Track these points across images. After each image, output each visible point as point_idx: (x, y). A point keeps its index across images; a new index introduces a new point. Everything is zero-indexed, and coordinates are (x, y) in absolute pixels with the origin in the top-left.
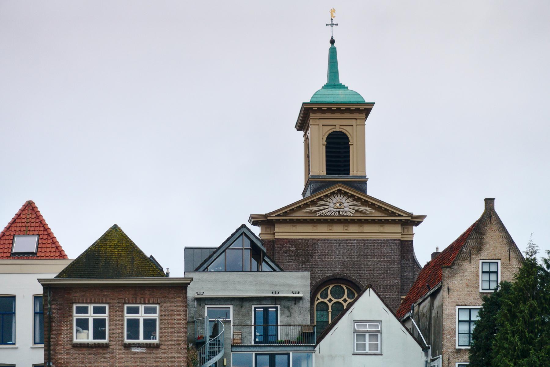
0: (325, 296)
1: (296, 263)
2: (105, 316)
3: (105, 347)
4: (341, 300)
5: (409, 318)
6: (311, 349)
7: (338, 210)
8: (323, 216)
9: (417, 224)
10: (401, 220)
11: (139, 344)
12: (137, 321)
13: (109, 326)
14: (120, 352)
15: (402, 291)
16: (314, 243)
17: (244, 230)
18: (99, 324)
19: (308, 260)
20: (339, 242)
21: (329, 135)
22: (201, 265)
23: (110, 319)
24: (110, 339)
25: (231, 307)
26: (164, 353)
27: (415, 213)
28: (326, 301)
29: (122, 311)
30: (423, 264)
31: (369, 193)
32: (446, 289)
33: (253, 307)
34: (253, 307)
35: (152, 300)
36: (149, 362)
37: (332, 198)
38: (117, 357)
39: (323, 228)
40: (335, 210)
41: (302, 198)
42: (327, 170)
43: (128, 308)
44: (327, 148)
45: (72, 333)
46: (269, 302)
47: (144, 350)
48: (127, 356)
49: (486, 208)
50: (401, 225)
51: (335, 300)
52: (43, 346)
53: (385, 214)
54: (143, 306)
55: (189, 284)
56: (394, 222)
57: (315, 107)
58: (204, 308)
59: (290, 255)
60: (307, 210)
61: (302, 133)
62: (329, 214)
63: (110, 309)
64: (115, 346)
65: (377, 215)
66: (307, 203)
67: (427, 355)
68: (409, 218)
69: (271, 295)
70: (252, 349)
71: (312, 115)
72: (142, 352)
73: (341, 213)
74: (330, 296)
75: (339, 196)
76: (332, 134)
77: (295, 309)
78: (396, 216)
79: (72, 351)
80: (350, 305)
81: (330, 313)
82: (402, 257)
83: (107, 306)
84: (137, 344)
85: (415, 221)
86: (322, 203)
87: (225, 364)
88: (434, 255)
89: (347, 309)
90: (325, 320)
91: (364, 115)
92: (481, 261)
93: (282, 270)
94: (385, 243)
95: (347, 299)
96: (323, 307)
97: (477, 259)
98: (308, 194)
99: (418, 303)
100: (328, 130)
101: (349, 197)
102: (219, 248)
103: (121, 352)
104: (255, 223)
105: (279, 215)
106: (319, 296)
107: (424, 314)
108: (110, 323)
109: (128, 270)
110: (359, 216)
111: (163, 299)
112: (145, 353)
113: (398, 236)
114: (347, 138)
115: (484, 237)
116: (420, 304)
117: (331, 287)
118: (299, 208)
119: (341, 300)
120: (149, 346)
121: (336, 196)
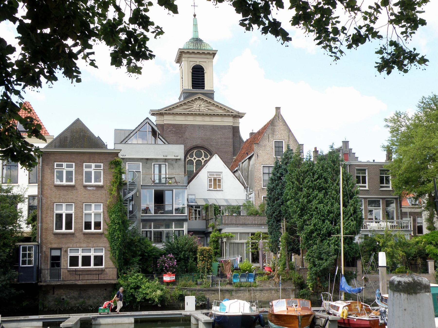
0: (192, 156)
3: (73, 187)
4: (200, 159)
5: (237, 170)
6: (185, 187)
7: (198, 108)
8: (190, 112)
9: (241, 117)
10: (233, 115)
13: (75, 175)
15: (234, 154)
16: (186, 126)
17: (147, 120)
18: (69, 174)
19: (182, 136)
20: (199, 126)
22: (124, 140)
23: (75, 171)
24: (75, 183)
25: (141, 163)
27: (240, 112)
28: (192, 159)
29: (83, 167)
30: (245, 140)
31: (215, 99)
32: (256, 156)
33: (153, 163)
34: (153, 163)
35: (99, 161)
36: (97, 195)
37: (195, 101)
38: (79, 192)
39: (190, 118)
40: (197, 108)
41: (178, 101)
43: (85, 165)
44: (192, 73)
45: (54, 178)
46: (162, 161)
47: (94, 188)
48: (85, 192)
49: (276, 112)
50: (233, 118)
51: (197, 159)
52: (37, 184)
53: (224, 111)
55: (119, 152)
57: (186, 51)
58: (126, 164)
60: (182, 108)
61: (178, 64)
63: (75, 165)
64: (79, 187)
65: (220, 112)
66: (181, 104)
67: (247, 191)
68: (237, 114)
69: (163, 157)
70: (152, 187)
71: (184, 55)
72: (93, 190)
73: (200, 110)
74: (194, 157)
75: (199, 100)
76: (185, 153)
77: (176, 165)
78: (230, 113)
79: (54, 189)
80: (206, 162)
81: (195, 166)
82: (234, 135)
83: (74, 164)
86: (190, 104)
87: (138, 196)
88: (251, 134)
89: (204, 165)
90: (192, 170)
91: (212, 56)
93: (169, 144)
94: (224, 127)
95: (204, 158)
96: (191, 162)
97: (272, 139)
98: (182, 99)
99: (242, 162)
100: (193, 64)
101: (204, 101)
102: (134, 130)
103: (81, 190)
104: (153, 114)
105: (166, 110)
106: (188, 156)
107: (245, 169)
108: (75, 173)
110: (210, 112)
111: (105, 160)
112: (95, 190)
113: (231, 124)
114: (203, 69)
115: (276, 128)
116: (243, 163)
117: (195, 151)
119: (200, 159)
121: (197, 101)
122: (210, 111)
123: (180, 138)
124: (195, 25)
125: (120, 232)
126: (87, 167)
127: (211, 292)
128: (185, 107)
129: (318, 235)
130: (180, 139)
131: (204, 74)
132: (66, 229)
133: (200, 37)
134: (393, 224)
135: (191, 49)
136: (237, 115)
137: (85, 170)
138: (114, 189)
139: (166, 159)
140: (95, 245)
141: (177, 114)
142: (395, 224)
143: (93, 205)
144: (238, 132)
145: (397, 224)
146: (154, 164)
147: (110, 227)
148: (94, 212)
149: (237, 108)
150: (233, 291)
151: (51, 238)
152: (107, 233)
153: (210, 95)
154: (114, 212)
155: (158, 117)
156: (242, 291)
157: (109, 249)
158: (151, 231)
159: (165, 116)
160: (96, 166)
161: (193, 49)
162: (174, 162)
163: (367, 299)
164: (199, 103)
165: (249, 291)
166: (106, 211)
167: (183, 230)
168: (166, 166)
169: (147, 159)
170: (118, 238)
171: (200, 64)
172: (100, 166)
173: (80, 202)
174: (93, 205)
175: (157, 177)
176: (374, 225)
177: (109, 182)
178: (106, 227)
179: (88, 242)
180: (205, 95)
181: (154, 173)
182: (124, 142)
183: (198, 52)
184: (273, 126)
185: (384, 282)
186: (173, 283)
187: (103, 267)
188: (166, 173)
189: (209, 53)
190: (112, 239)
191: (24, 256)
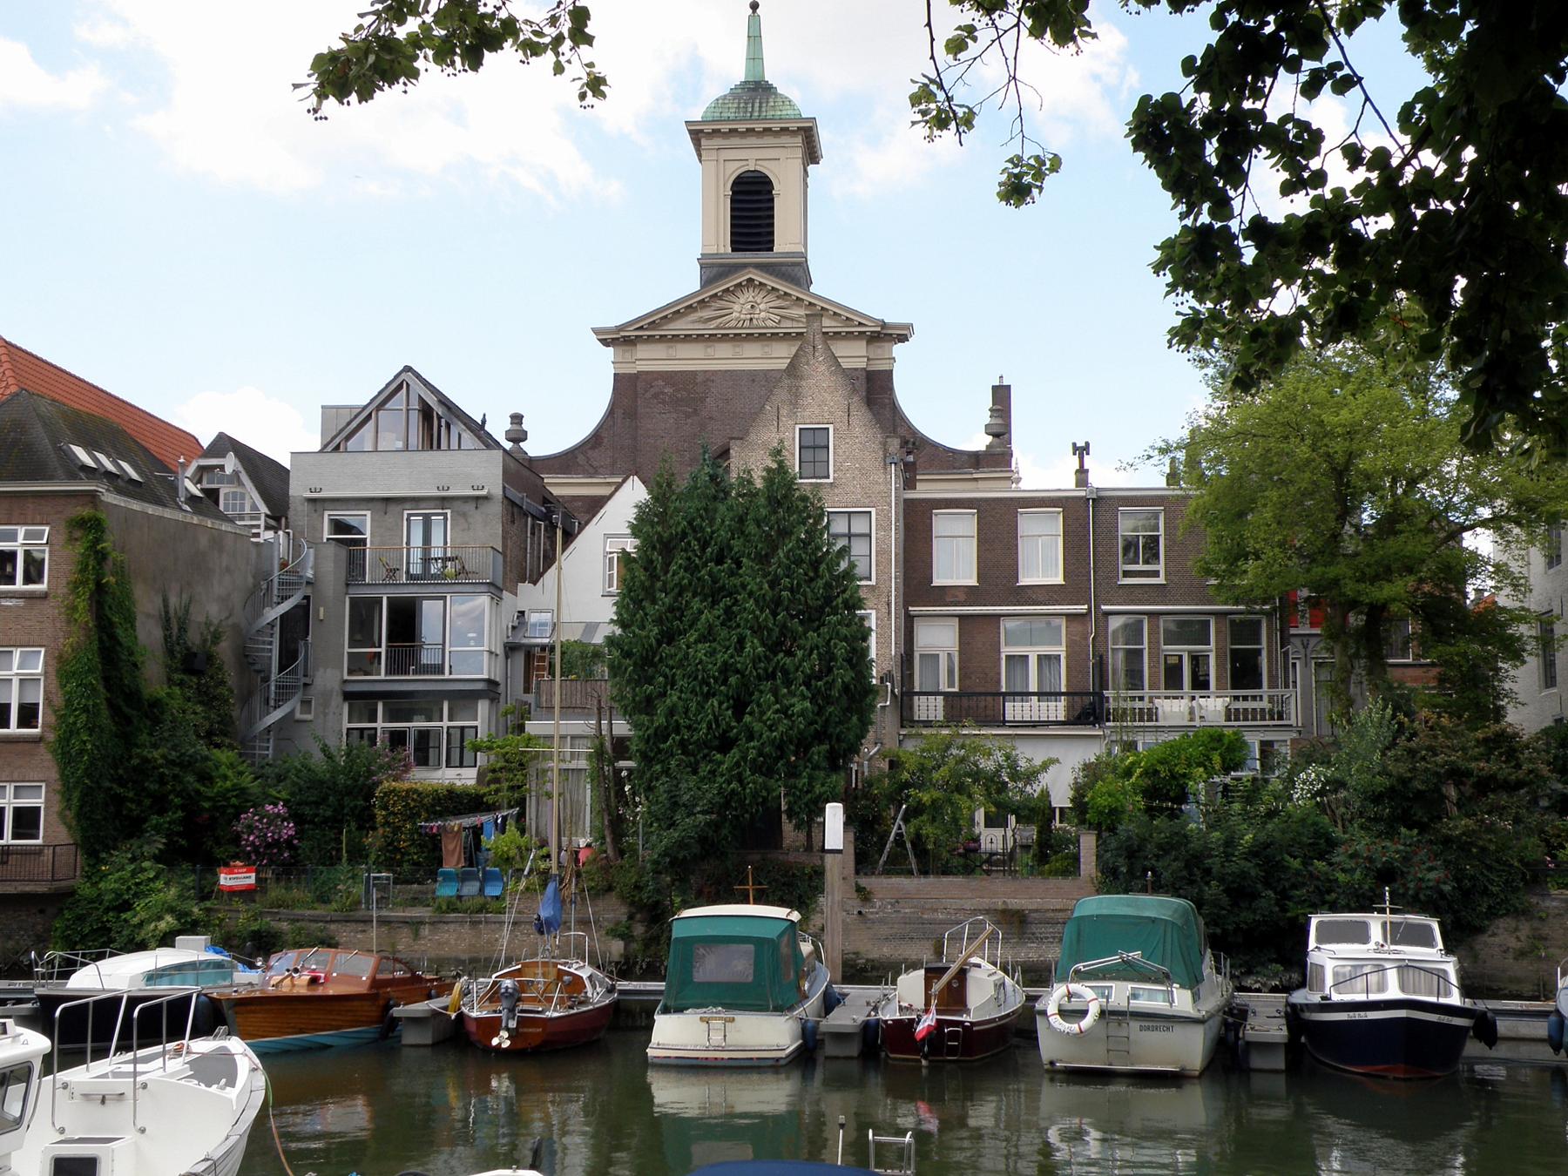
1: (675, 415)
9: (903, 338)
11: (15, 592)
16: (710, 376)
21: (738, 177)
25: (368, 513)
34: (406, 512)
36: (28, 623)
37: (739, 294)
39: (724, 350)
42: (732, 242)
44: (732, 201)
46: (432, 504)
47: (21, 603)
50: (868, 343)
54: (24, 528)
59: (664, 402)
62: (733, 324)
66: (691, 306)
75: (751, 290)
77: (477, 517)
84: (9, 592)
85: (901, 335)
100: (733, 171)
101: (769, 292)
105: (641, 328)
112: (23, 608)
113: (864, 365)
118: (690, 309)
122: (788, 324)
123: (688, 416)
124: (755, 38)
125: (90, 735)
127: (353, 926)
128: (706, 314)
129: (683, 744)
130: (689, 421)
131: (772, 200)
132: (21, 724)
133: (769, 77)
135: (728, 120)
136: (879, 332)
138: (82, 605)
139: (444, 499)
140: (16, 776)
141: (675, 338)
143: (17, 653)
146: (409, 515)
147: (61, 718)
148: (17, 674)
150: (422, 923)
152: (51, 737)
153: (795, 272)
154: (74, 673)
155: (620, 349)
156: (452, 926)
157: (58, 787)
159: (639, 347)
160: (28, 536)
162: (470, 507)
163: (867, 960)
164: (751, 299)
165: (474, 924)
166: (52, 671)
167: (476, 727)
168: (446, 519)
169: (387, 500)
170: (81, 752)
171: (758, 168)
172: (40, 535)
174: (17, 653)
175: (416, 555)
176: (1176, 709)
177: (64, 582)
178: (52, 719)
181: (408, 543)
182: (329, 448)
183: (766, 130)
184: (796, 377)
185: (833, 902)
186: (246, 894)
187: (39, 841)
188: (445, 543)
189: (784, 130)
190: (66, 756)
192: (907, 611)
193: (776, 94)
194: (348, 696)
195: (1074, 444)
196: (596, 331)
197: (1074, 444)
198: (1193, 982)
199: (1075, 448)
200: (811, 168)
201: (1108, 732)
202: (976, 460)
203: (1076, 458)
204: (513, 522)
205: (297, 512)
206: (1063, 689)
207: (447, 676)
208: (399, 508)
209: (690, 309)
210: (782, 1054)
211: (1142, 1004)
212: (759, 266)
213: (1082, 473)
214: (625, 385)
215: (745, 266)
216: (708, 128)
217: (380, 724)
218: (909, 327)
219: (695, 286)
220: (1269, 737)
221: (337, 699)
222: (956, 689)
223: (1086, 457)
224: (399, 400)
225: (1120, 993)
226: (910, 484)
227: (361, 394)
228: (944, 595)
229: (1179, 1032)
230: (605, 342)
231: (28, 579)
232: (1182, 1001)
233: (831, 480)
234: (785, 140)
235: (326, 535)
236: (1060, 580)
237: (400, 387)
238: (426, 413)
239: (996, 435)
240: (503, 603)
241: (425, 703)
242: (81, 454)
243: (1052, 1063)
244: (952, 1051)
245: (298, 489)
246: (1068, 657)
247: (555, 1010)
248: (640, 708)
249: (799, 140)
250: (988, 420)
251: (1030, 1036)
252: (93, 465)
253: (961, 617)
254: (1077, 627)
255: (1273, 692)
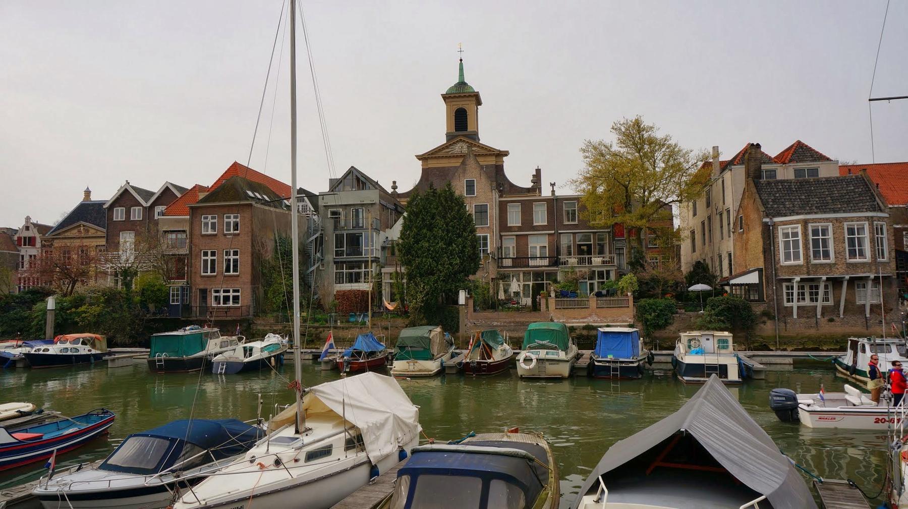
2: (215, 221)
9: (506, 155)
12: (230, 222)
14: (222, 238)
18: (213, 225)
21: (457, 110)
26: (241, 238)
56: (490, 155)
62: (456, 153)
65: (440, 154)
69: (359, 203)
79: (201, 238)
85: (506, 154)
92: (465, 180)
100: (455, 108)
109: (809, 154)
113: (494, 163)
114: (466, 111)
118: (443, 149)
120: (235, 235)
123: (443, 180)
124: (461, 69)
126: (205, 218)
131: (467, 116)
134: (605, 259)
135: (453, 93)
137: (226, 220)
139: (363, 204)
142: (607, 259)
144: (502, 170)
145: (609, 260)
149: (499, 146)
151: (198, 280)
153: (474, 136)
158: (343, 272)
161: (456, 93)
168: (363, 211)
173: (221, 248)
179: (227, 284)
180: (466, 137)
183: (459, 96)
187: (239, 305)
191: (173, 296)
192: (500, 234)
193: (468, 85)
194: (335, 263)
195: (551, 183)
196: (417, 156)
197: (551, 183)
198: (566, 349)
199: (551, 184)
200: (479, 107)
201: (560, 268)
202: (528, 190)
203: (551, 187)
204: (383, 211)
205: (321, 210)
206: (547, 256)
207: (363, 256)
208: (350, 207)
209: (443, 149)
210: (432, 373)
211: (550, 357)
212: (463, 135)
213: (553, 191)
214: (426, 172)
215: (459, 135)
216: (447, 96)
217: (345, 271)
218: (508, 152)
219: (444, 141)
220: (608, 269)
221: (332, 264)
222: (515, 257)
223: (554, 187)
224: (350, 177)
225: (542, 354)
226: (501, 196)
227: (339, 176)
228: (510, 229)
229: (561, 365)
230: (419, 159)
231: (235, 230)
232: (562, 355)
233: (475, 195)
234: (470, 99)
235: (329, 216)
236: (546, 224)
237: (350, 172)
238: (358, 179)
239: (534, 183)
240: (380, 234)
241: (358, 264)
242: (250, 193)
243: (521, 376)
244: (484, 371)
245: (321, 203)
246: (548, 247)
247: (362, 359)
248: (408, 263)
249: (474, 99)
250: (532, 179)
251: (515, 367)
252: (253, 196)
253: (517, 235)
254: (551, 238)
255: (611, 255)
